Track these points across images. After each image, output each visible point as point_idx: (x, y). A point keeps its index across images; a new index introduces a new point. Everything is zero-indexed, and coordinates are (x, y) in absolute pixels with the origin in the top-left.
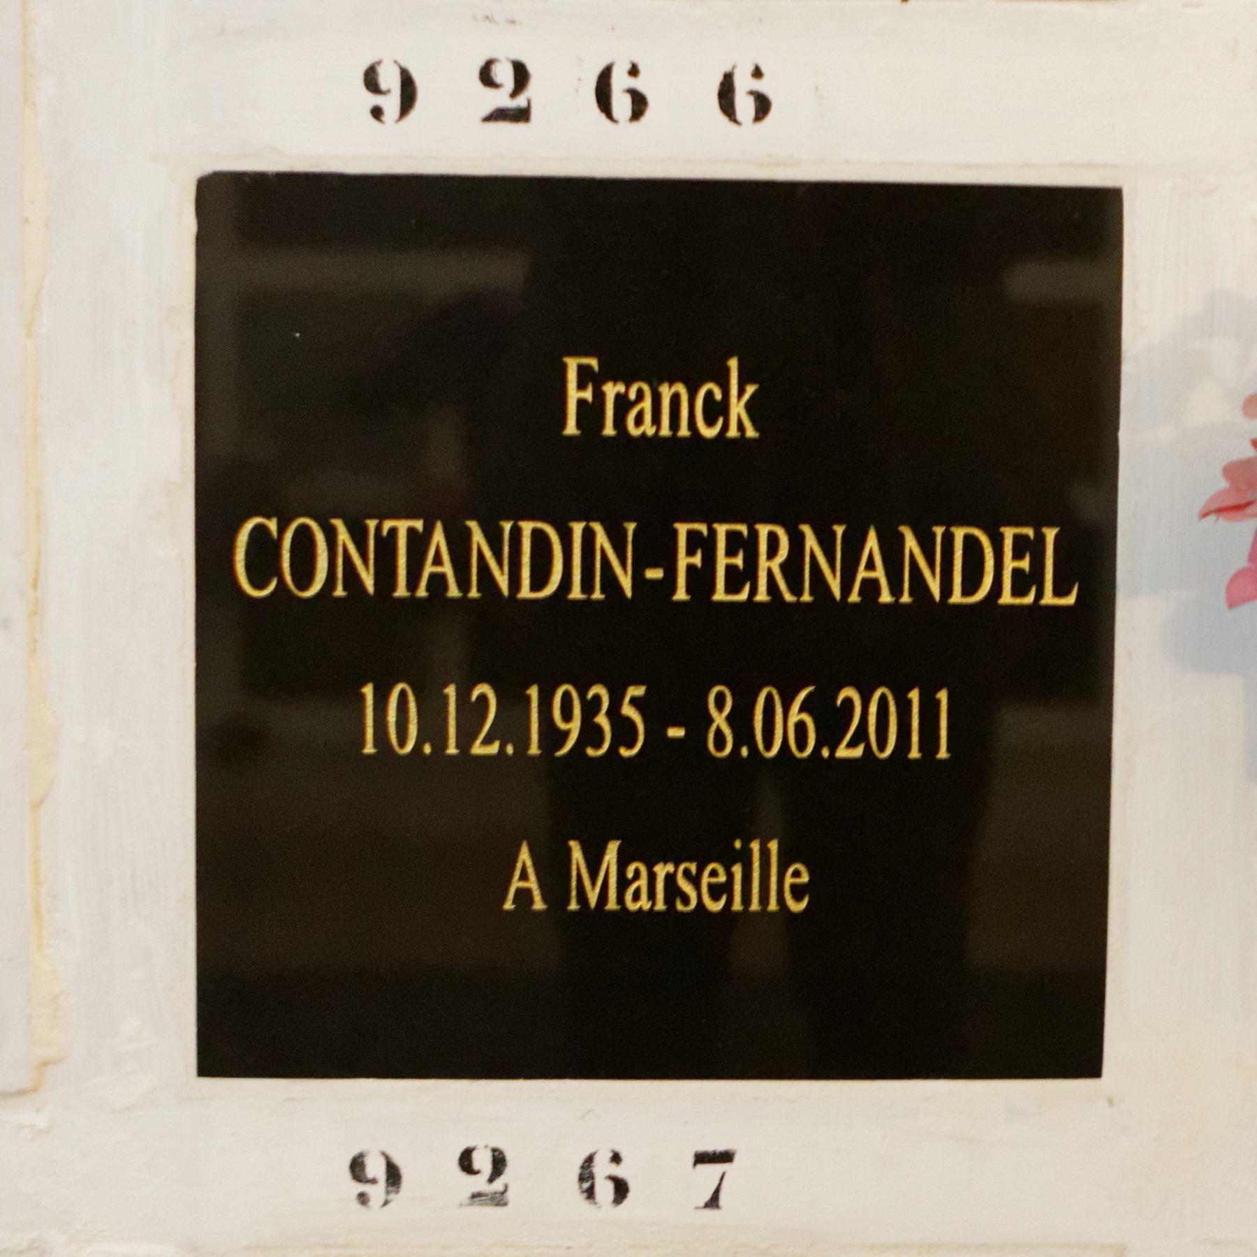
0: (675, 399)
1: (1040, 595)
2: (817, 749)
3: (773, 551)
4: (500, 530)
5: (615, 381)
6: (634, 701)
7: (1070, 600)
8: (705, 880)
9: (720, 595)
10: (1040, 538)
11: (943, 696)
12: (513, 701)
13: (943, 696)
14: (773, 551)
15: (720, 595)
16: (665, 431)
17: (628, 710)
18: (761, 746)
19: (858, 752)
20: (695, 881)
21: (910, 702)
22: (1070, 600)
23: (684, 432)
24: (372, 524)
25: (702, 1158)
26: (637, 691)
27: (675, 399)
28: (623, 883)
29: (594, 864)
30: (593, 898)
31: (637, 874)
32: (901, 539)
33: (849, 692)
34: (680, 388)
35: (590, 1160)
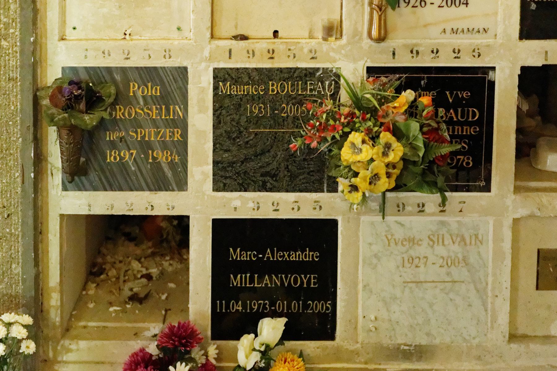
0: (299, 255)
1: (254, 284)
2: (325, 311)
4: (288, 276)
5: (250, 251)
6: (329, 304)
7: (317, 286)
9: (312, 286)
11: (224, 302)
13: (224, 302)
14: (178, 133)
15: (312, 286)
16: (297, 259)
17: (328, 305)
18: (232, 310)
19: (260, 302)
21: (300, 304)
22: (317, 286)
23: (301, 259)
24: (263, 286)
26: (330, 302)
27: (299, 255)
28: (241, 255)
29: (235, 251)
30: (235, 258)
31: (244, 254)
32: (272, 277)
33: (310, 302)
34: (300, 252)
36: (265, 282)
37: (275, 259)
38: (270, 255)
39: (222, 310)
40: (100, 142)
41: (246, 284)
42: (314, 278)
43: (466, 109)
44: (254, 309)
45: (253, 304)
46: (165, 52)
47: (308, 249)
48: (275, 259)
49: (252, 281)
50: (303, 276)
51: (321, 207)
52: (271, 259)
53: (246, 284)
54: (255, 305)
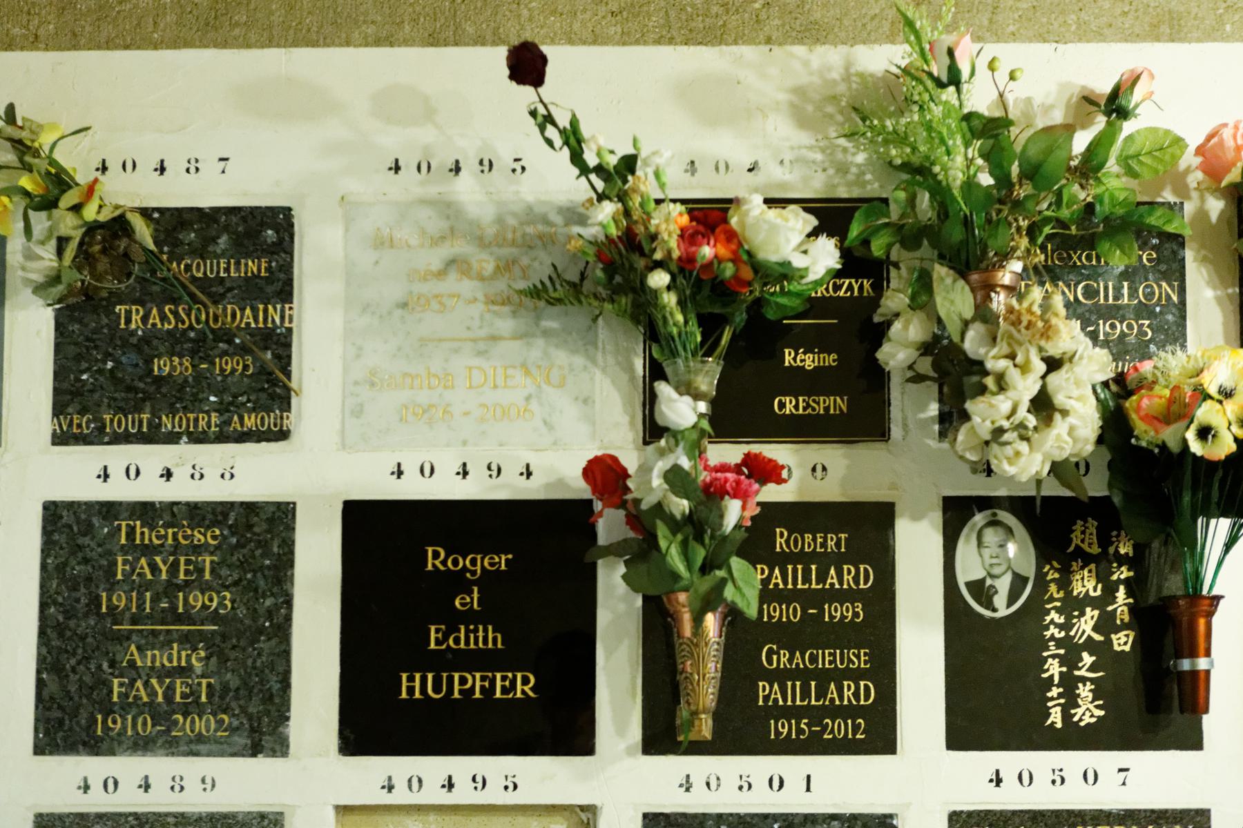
3: (849, 689)
8: (209, 534)
10: (835, 653)
12: (238, 263)
14: (849, 689)
19: (831, 736)
20: (205, 535)
24: (827, 703)
25: (1120, 770)
35: (1030, 783)
36: (829, 696)
37: (846, 702)
38: (779, 696)
39: (434, 678)
40: (687, 511)
41: (794, 700)
42: (865, 654)
43: (445, 675)
44: (782, 733)
45: (780, 724)
46: (189, 162)
47: (478, 695)
48: (846, 702)
49: (806, 694)
50: (802, 666)
51: (523, 168)
52: (837, 703)
53: (794, 700)
54: (783, 727)
